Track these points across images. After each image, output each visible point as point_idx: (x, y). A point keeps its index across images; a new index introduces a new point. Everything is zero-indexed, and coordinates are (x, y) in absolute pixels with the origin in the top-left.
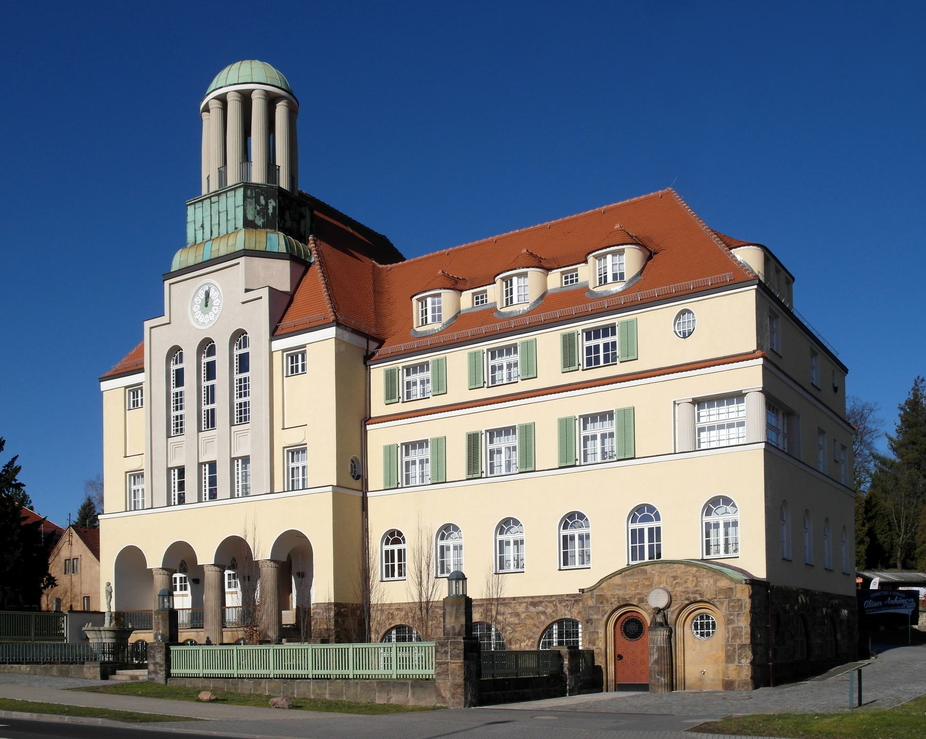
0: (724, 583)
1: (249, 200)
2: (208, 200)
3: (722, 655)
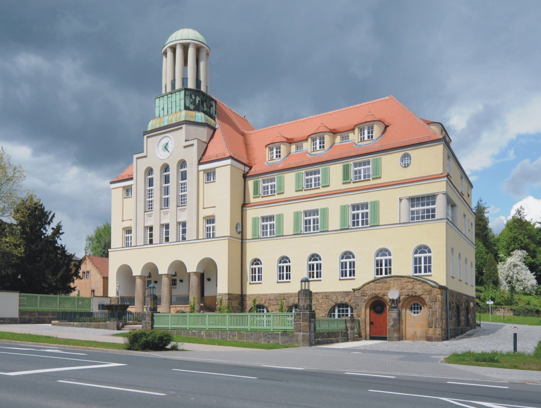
0: (427, 287)
2: (166, 96)
3: (426, 324)
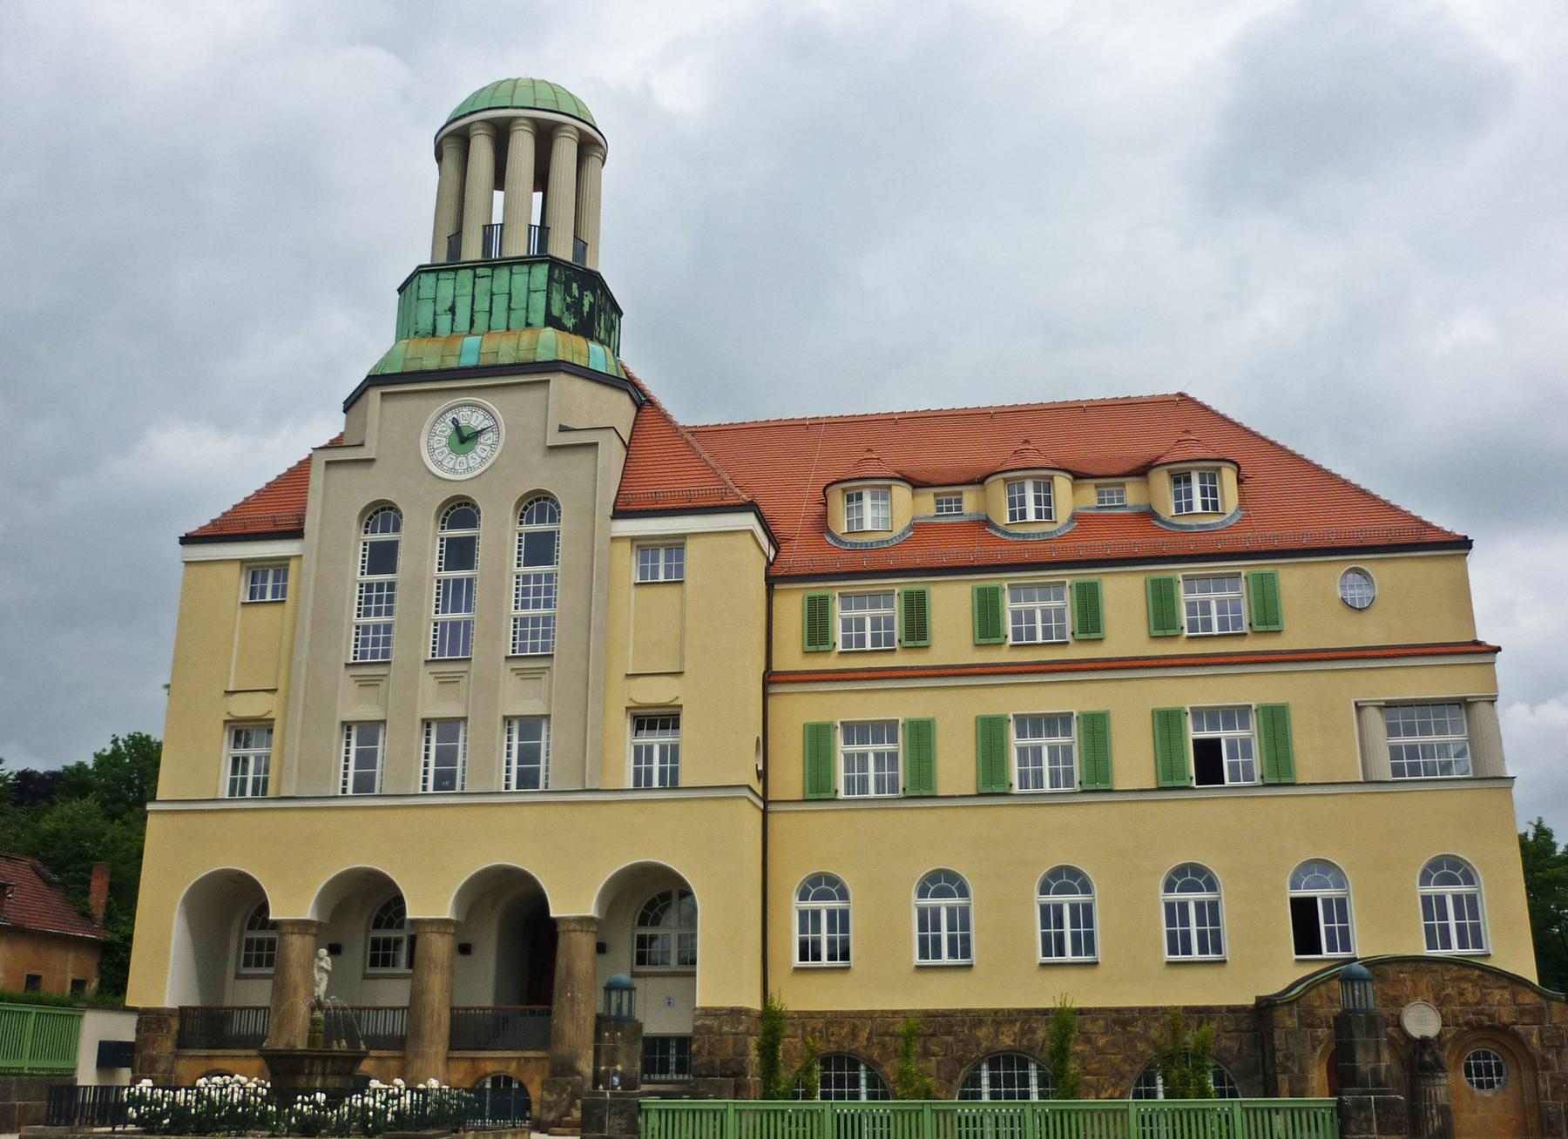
1: (554, 284)
2: (470, 273)
